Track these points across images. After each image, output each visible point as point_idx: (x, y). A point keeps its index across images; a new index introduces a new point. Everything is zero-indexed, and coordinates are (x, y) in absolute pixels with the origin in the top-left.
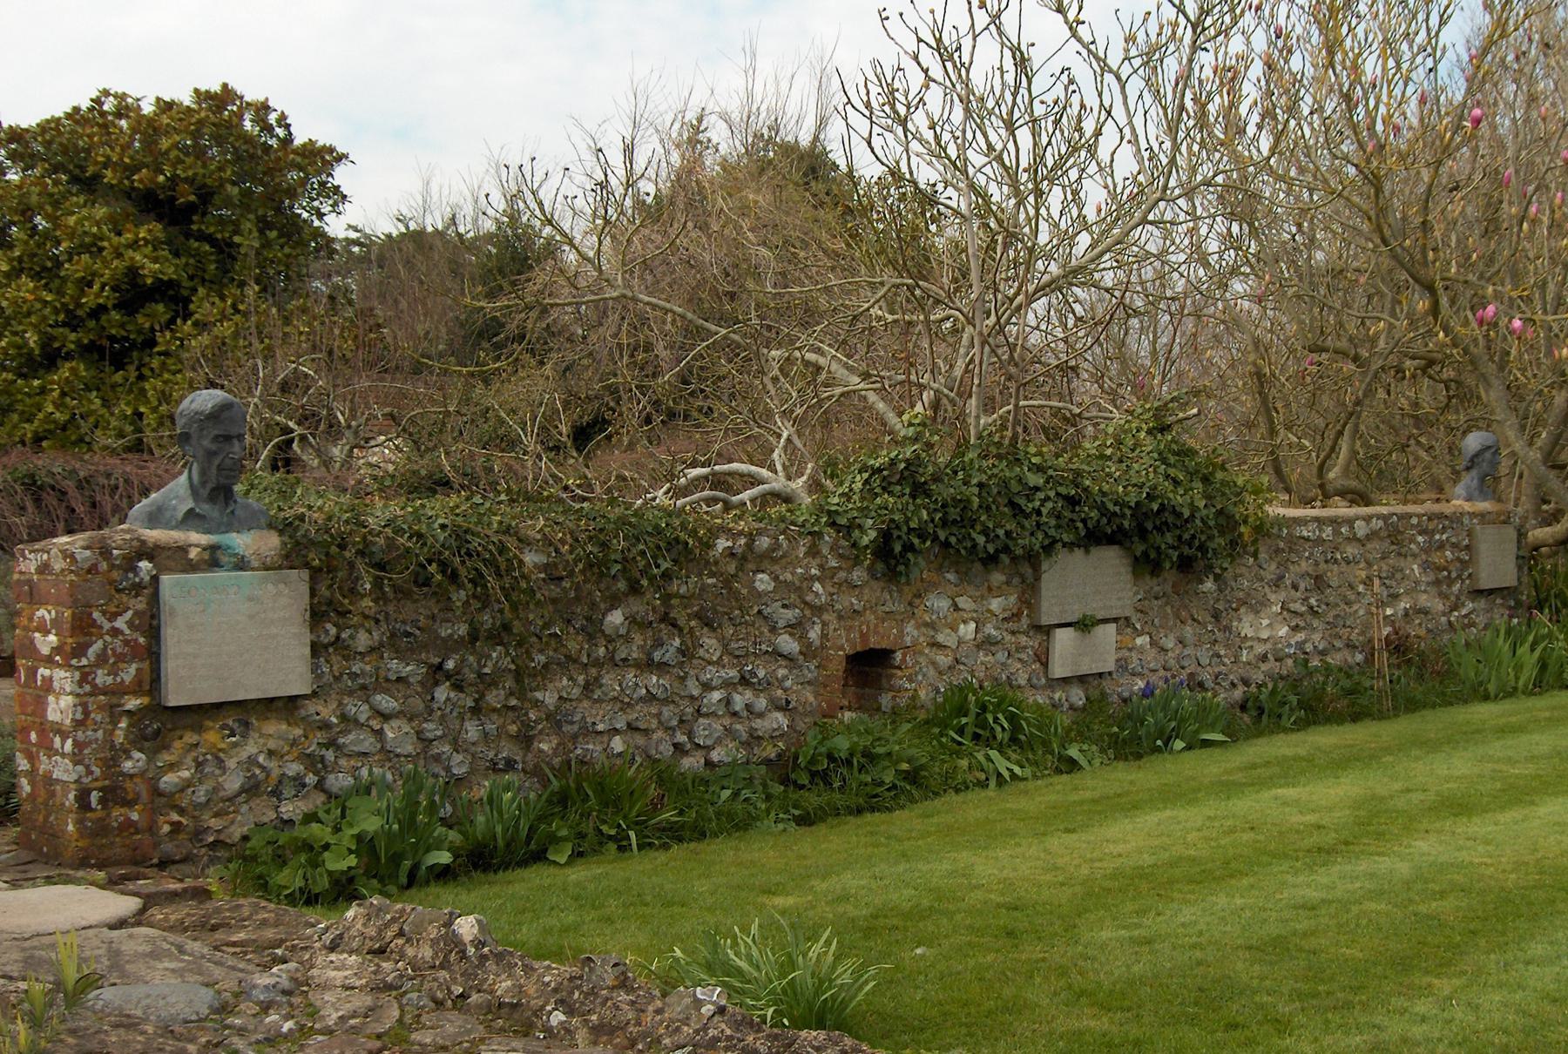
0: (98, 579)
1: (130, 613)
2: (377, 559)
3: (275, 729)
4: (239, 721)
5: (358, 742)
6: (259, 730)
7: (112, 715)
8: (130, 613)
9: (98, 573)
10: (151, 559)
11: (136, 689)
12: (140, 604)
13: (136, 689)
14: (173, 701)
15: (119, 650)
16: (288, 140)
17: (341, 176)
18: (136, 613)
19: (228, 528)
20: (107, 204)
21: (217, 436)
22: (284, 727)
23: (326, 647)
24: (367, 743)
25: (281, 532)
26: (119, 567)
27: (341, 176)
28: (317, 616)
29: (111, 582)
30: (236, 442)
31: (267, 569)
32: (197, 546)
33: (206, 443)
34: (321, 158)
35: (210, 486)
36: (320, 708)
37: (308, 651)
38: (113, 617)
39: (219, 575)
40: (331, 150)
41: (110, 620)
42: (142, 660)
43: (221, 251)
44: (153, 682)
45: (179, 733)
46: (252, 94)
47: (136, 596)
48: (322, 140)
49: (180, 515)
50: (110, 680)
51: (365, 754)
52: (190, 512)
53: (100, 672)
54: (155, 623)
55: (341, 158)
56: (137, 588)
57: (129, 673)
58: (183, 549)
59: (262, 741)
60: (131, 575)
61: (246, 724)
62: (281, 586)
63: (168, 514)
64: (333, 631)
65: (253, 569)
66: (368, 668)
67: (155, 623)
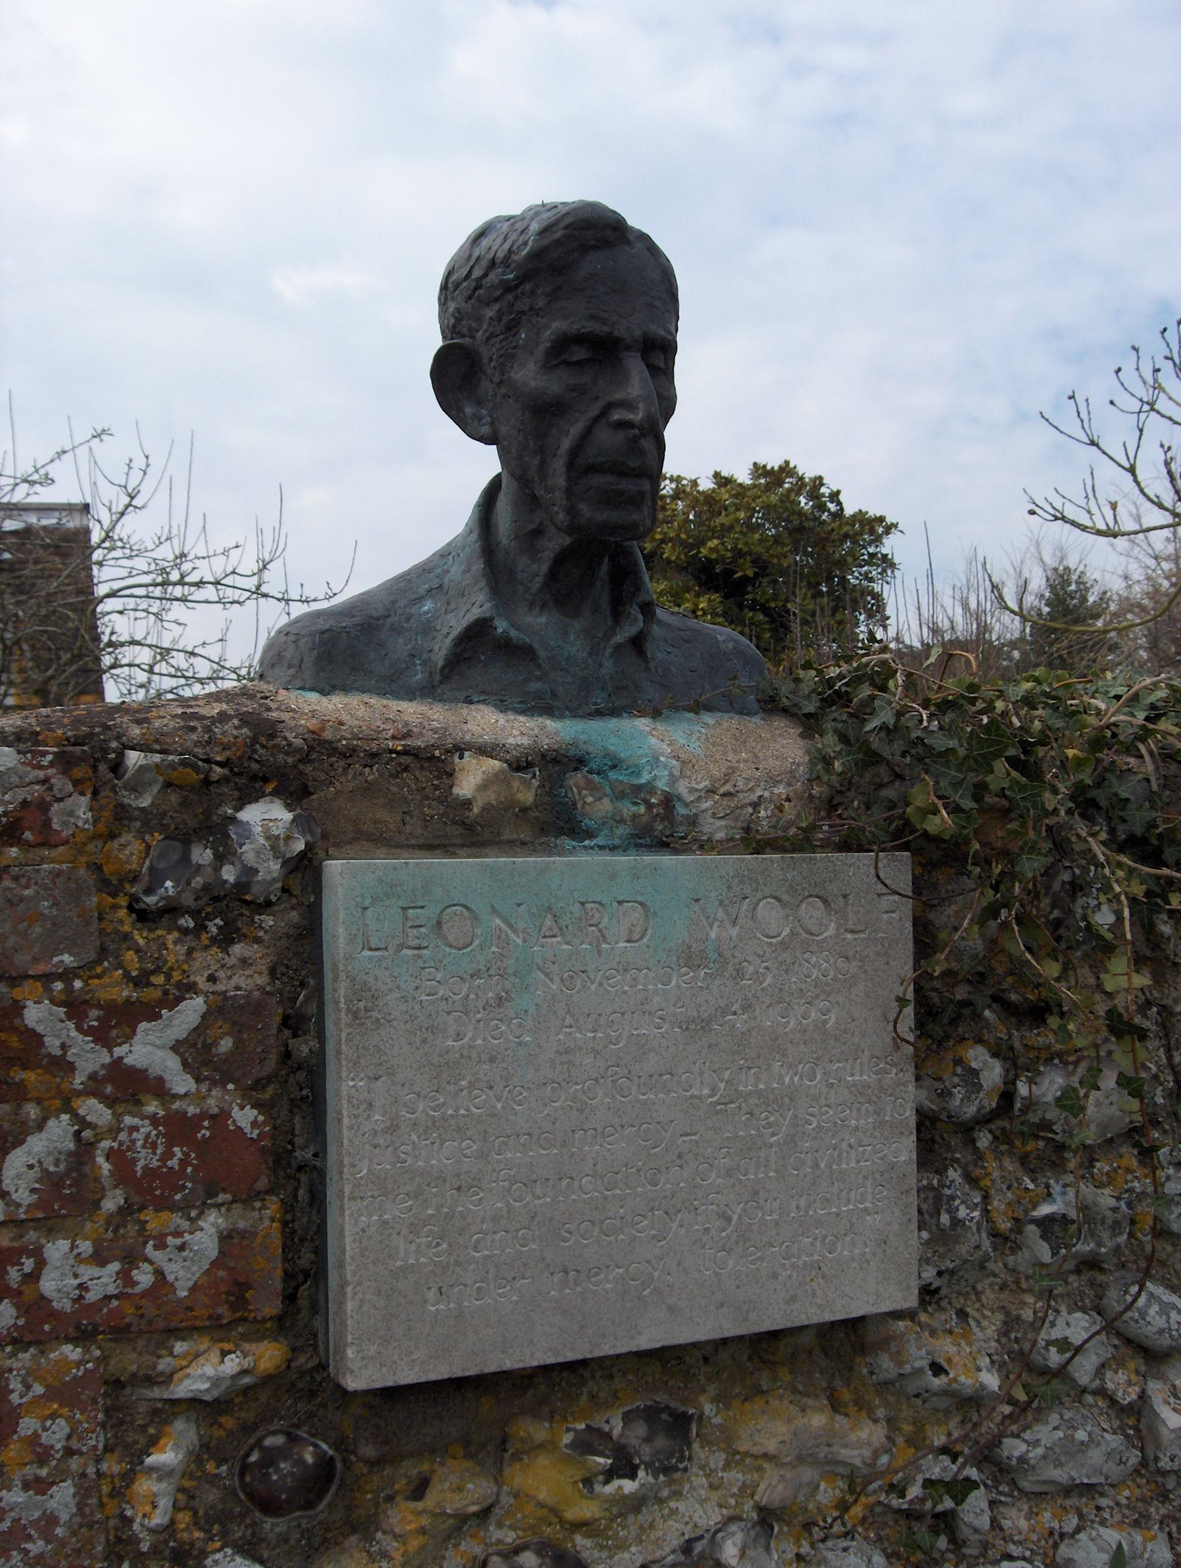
0: (52, 862)
1: (192, 1010)
2: (1137, 819)
3: (781, 1427)
4: (650, 1414)
5: (1072, 1450)
6: (727, 1439)
7: (117, 1417)
8: (192, 1010)
9: (47, 839)
10: (294, 792)
11: (225, 1310)
12: (244, 970)
13: (225, 1310)
14: (362, 1369)
15: (145, 1159)
16: (839, 514)
17: (890, 545)
18: (221, 1010)
19: (620, 702)
20: (666, 578)
21: (563, 343)
22: (818, 1420)
23: (967, 1130)
24: (1102, 1450)
25: (810, 725)
26: (148, 820)
27: (890, 545)
28: (937, 1019)
29: (110, 883)
30: (635, 367)
31: (759, 847)
32: (484, 751)
33: (528, 374)
34: (872, 527)
35: (555, 542)
36: (945, 1347)
37: (905, 1150)
38: (118, 1021)
39: (570, 869)
40: (881, 519)
41: (102, 1037)
42: (248, 1198)
43: (773, 621)
44: (294, 1287)
45: (412, 1469)
46: (808, 471)
47: (226, 939)
48: (873, 511)
49: (441, 648)
50: (103, 1280)
51: (1088, 1489)
52: (477, 632)
53: (57, 1250)
54: (303, 1048)
55: (889, 529)
56: (228, 910)
57: (190, 1251)
58: (433, 762)
59: (735, 1477)
60: (202, 855)
61: (678, 1425)
62: (812, 912)
63: (400, 647)
64: (993, 1073)
65: (706, 846)
66: (1105, 1199)
67: (303, 1048)
